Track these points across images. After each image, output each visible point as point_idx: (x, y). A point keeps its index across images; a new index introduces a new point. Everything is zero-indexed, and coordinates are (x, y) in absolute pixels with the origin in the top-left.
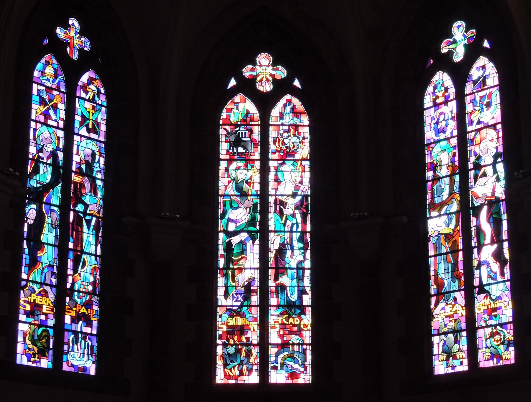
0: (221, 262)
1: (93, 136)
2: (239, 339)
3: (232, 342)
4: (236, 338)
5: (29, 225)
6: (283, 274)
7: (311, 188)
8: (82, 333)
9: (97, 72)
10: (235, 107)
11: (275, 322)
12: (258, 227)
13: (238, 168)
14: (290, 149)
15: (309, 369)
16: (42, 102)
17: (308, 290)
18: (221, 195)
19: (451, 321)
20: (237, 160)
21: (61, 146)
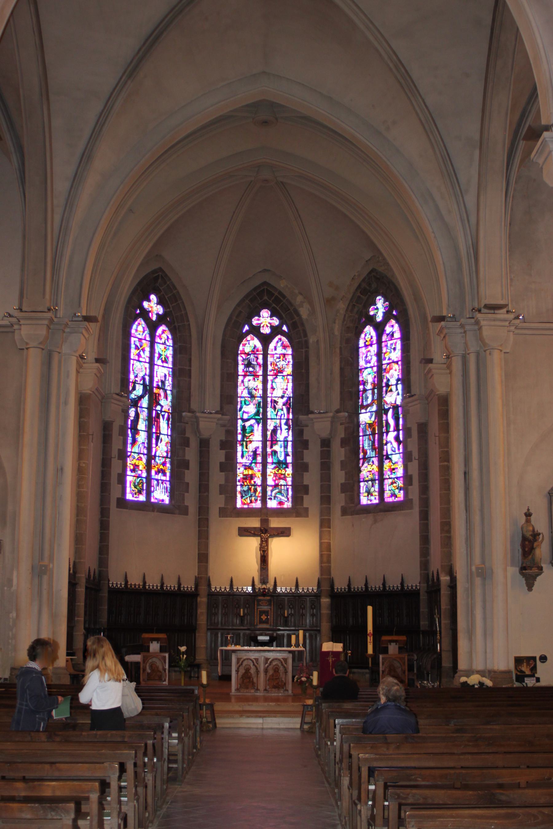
0: (239, 437)
1: (165, 365)
2: (250, 482)
3: (246, 484)
4: (248, 481)
5: (131, 421)
6: (276, 444)
7: (293, 392)
8: (161, 480)
9: (167, 326)
10: (248, 343)
11: (271, 472)
12: (261, 416)
13: (249, 380)
14: (280, 369)
15: (290, 499)
16: (137, 348)
17: (290, 454)
18: (239, 397)
19: (370, 474)
20: (249, 375)
21: (148, 373)
